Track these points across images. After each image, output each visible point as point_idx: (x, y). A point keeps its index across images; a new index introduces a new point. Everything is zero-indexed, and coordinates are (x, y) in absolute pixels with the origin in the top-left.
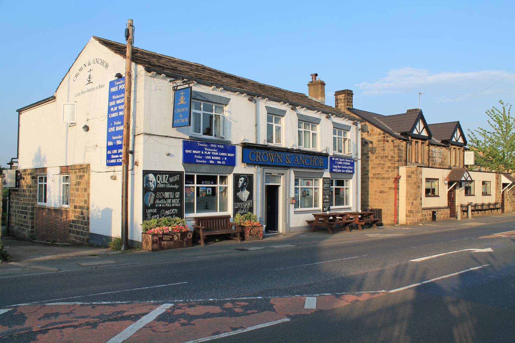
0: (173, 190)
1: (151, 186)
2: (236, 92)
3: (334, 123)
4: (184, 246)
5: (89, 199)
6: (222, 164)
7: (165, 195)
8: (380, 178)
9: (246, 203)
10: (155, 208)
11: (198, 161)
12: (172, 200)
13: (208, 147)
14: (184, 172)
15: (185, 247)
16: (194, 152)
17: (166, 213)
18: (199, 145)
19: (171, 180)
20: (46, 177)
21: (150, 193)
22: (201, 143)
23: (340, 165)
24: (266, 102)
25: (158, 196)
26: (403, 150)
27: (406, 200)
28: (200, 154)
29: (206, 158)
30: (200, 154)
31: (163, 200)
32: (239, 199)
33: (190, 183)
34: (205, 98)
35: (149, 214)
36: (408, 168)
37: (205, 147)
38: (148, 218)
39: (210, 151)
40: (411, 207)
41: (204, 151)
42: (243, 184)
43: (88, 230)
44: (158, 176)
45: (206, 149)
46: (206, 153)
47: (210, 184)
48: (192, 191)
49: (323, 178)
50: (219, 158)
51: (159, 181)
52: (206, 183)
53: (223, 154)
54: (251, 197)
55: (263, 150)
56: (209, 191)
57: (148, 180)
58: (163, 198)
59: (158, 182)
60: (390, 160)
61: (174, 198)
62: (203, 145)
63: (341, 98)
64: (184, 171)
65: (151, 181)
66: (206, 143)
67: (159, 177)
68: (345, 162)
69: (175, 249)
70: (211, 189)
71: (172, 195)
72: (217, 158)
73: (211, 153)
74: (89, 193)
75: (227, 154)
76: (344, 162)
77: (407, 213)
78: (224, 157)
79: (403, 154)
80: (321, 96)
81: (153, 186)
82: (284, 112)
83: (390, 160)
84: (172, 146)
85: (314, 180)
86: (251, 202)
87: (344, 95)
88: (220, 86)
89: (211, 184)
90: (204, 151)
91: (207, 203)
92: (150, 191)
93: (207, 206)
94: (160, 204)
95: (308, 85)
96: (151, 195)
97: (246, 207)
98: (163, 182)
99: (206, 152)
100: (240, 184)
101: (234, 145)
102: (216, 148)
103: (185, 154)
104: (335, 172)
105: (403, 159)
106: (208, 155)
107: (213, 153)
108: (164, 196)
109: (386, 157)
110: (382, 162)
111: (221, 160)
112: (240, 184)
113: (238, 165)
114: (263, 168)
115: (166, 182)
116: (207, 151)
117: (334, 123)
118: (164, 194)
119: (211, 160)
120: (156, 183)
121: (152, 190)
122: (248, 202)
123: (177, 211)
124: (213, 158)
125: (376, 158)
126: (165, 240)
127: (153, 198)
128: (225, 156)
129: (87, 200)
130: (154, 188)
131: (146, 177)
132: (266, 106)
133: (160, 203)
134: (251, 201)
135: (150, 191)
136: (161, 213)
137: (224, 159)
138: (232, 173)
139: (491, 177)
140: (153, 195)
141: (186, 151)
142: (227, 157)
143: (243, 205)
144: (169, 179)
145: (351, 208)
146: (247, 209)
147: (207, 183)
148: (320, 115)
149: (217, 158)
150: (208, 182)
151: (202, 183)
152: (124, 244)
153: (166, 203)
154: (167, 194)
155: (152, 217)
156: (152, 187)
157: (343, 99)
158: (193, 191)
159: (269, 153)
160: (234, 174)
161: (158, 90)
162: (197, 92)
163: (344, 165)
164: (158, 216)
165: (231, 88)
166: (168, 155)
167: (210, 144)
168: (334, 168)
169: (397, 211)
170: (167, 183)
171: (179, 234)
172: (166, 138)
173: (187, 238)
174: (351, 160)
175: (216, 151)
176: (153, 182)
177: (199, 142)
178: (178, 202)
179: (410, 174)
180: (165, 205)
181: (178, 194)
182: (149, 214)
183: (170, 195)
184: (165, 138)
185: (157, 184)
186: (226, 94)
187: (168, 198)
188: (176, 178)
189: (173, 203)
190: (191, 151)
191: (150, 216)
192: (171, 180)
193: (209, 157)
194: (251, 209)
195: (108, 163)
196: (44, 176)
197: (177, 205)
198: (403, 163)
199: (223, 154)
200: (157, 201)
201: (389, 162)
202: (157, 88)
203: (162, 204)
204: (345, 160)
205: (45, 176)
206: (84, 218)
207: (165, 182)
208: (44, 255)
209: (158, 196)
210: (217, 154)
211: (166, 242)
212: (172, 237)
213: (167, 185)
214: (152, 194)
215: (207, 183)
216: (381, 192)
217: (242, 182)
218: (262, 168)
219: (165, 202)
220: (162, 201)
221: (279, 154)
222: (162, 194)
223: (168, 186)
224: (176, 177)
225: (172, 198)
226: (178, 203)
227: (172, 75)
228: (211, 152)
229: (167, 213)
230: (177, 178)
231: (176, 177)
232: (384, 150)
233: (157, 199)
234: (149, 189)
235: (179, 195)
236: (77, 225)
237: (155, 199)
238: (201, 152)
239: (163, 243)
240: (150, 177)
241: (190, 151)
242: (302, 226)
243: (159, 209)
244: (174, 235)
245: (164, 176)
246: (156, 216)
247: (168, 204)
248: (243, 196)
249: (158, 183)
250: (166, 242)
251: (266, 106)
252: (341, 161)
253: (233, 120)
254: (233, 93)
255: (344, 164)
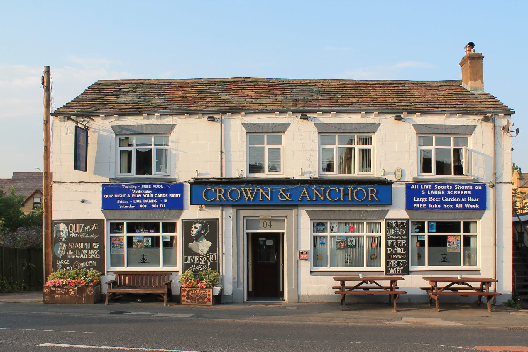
0: (91, 241)
1: (62, 236)
2: (184, 114)
3: (416, 126)
4: (84, 302)
6: (159, 208)
7: (79, 246)
9: (206, 257)
10: (67, 259)
11: (122, 207)
12: (88, 252)
13: (137, 189)
14: (104, 220)
15: (84, 303)
16: (116, 196)
17: (81, 265)
18: (123, 188)
19: (87, 229)
21: (61, 244)
22: (126, 185)
24: (243, 118)
25: (70, 247)
28: (126, 199)
29: (134, 202)
30: (126, 199)
31: (77, 251)
32: (193, 251)
33: (118, 232)
34: (134, 131)
35: (59, 265)
37: (133, 189)
38: (59, 270)
39: (140, 194)
41: (131, 194)
42: (199, 232)
44: (71, 225)
45: (134, 192)
46: (145, 196)
47: (148, 232)
48: (121, 241)
49: (386, 219)
50: (156, 201)
51: (72, 231)
52: (142, 231)
53: (162, 196)
54: (214, 249)
55: (228, 185)
56: (147, 241)
57: (58, 230)
58: (77, 249)
59: (71, 232)
61: (92, 249)
62: (130, 187)
64: (104, 218)
65: (62, 231)
66: (134, 185)
67: (71, 227)
70: (150, 239)
71: (89, 246)
72: (151, 201)
73: (142, 196)
75: (168, 195)
78: (163, 199)
80: (470, 80)
81: (65, 236)
82: (286, 126)
84: (88, 192)
85: (365, 223)
86: (214, 256)
88: (154, 112)
89: (151, 233)
90: (131, 194)
91: (144, 255)
92: (61, 241)
93: (144, 259)
94: (74, 255)
96: (62, 246)
97: (206, 261)
98: (77, 232)
99: (133, 196)
100: (193, 232)
101: (182, 182)
102: (149, 189)
103: (103, 199)
104: (416, 209)
106: (138, 199)
107: (144, 196)
108: (78, 246)
111: (158, 204)
112: (193, 232)
113: (189, 208)
114: (237, 210)
115: (81, 232)
116: (136, 194)
117: (416, 126)
118: (78, 245)
119: (143, 203)
120: (68, 233)
121: (63, 240)
122: (209, 255)
123: (95, 263)
124: (145, 201)
126: (58, 294)
127: (64, 248)
128: (165, 198)
130: (65, 238)
131: (56, 227)
132: (243, 124)
133: (72, 254)
134: (215, 255)
135: (61, 241)
136: (74, 265)
137: (163, 201)
138: (179, 218)
140: (65, 245)
141: (106, 196)
142: (168, 198)
143: (199, 259)
144: (84, 228)
145: (481, 271)
146: (207, 265)
147: (144, 232)
148: (375, 118)
149: (151, 201)
150: (145, 230)
151: (136, 231)
153: (81, 255)
154: (82, 245)
155: (63, 269)
156: (64, 237)
158: (459, 240)
159: (243, 189)
160: (182, 219)
161: (69, 133)
162: (122, 126)
164: (71, 268)
165: (172, 112)
166: (83, 202)
167: (140, 185)
170: (82, 233)
171: (76, 288)
172: (80, 183)
173: (87, 294)
174: (446, 185)
175: (149, 192)
176: (64, 232)
177: (123, 185)
178: (96, 253)
180: (80, 256)
181: (96, 245)
182: (59, 265)
183: (85, 246)
184: (79, 184)
185: (70, 233)
186: (167, 121)
187: (83, 249)
188: (94, 227)
189: (89, 255)
190: (112, 195)
191: (61, 268)
192: (87, 229)
193: (140, 201)
194: (215, 266)
195: (477, 206)
197: (94, 257)
199: (162, 196)
200: (70, 252)
202: (69, 132)
203: (75, 255)
207: (79, 232)
208: (253, 307)
209: (70, 247)
210: (152, 196)
211: (59, 295)
212: (67, 291)
213: (82, 235)
214: (63, 245)
215: (144, 231)
217: (198, 229)
218: (235, 210)
219: (79, 253)
220: (76, 252)
221: (262, 188)
222: (75, 244)
223: (84, 236)
224: (94, 226)
225: (88, 250)
226: (97, 255)
227: (82, 114)
228: (142, 194)
229: (82, 265)
230: (94, 227)
231: (94, 226)
233: (70, 250)
234: (59, 239)
235: (98, 246)
237: (67, 250)
238: (126, 196)
239: (56, 296)
240: (61, 227)
241: (111, 196)
242: (330, 294)
243: (72, 261)
244: (69, 288)
245: (78, 225)
246: (69, 268)
247: (83, 255)
248: (200, 248)
249: (71, 233)
250: (59, 296)
251: (243, 124)
253: (179, 151)
254: (180, 117)
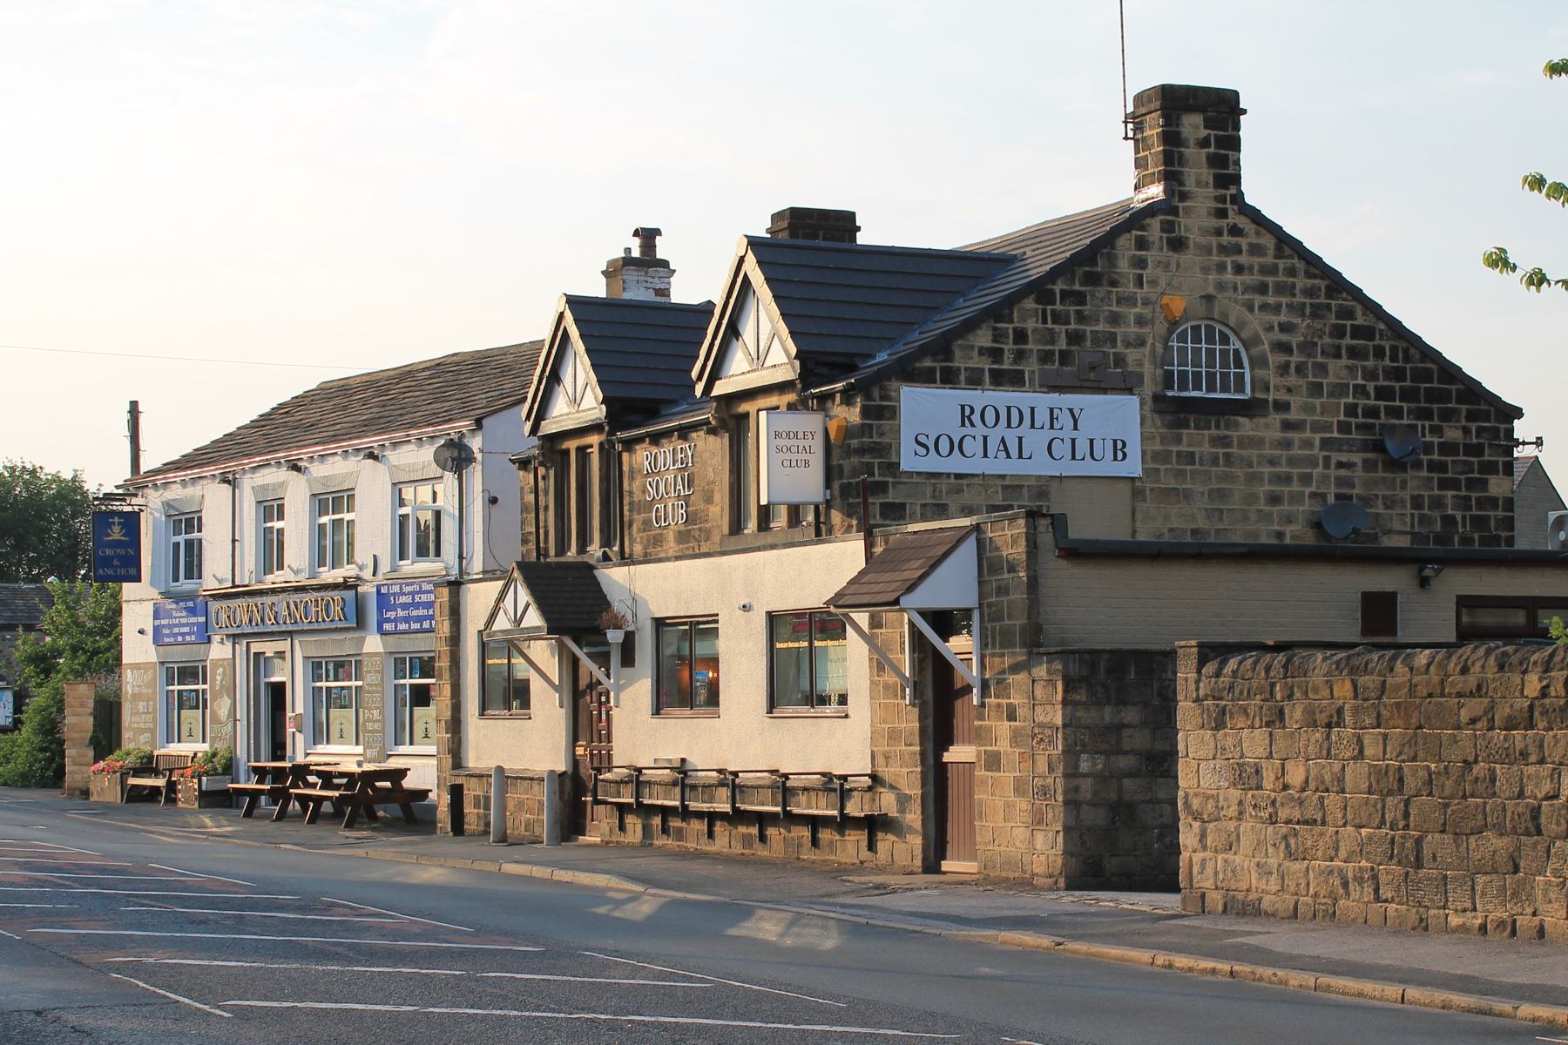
20: (283, 505)
23: (405, 606)
68: (420, 592)
69: (1519, 980)
76: (418, 593)
95: (602, 272)
163: (416, 606)
168: (388, 620)
169: (1171, 695)
196: (275, 504)
204: (421, 587)
205: (280, 502)
252: (409, 593)
255: (417, 600)
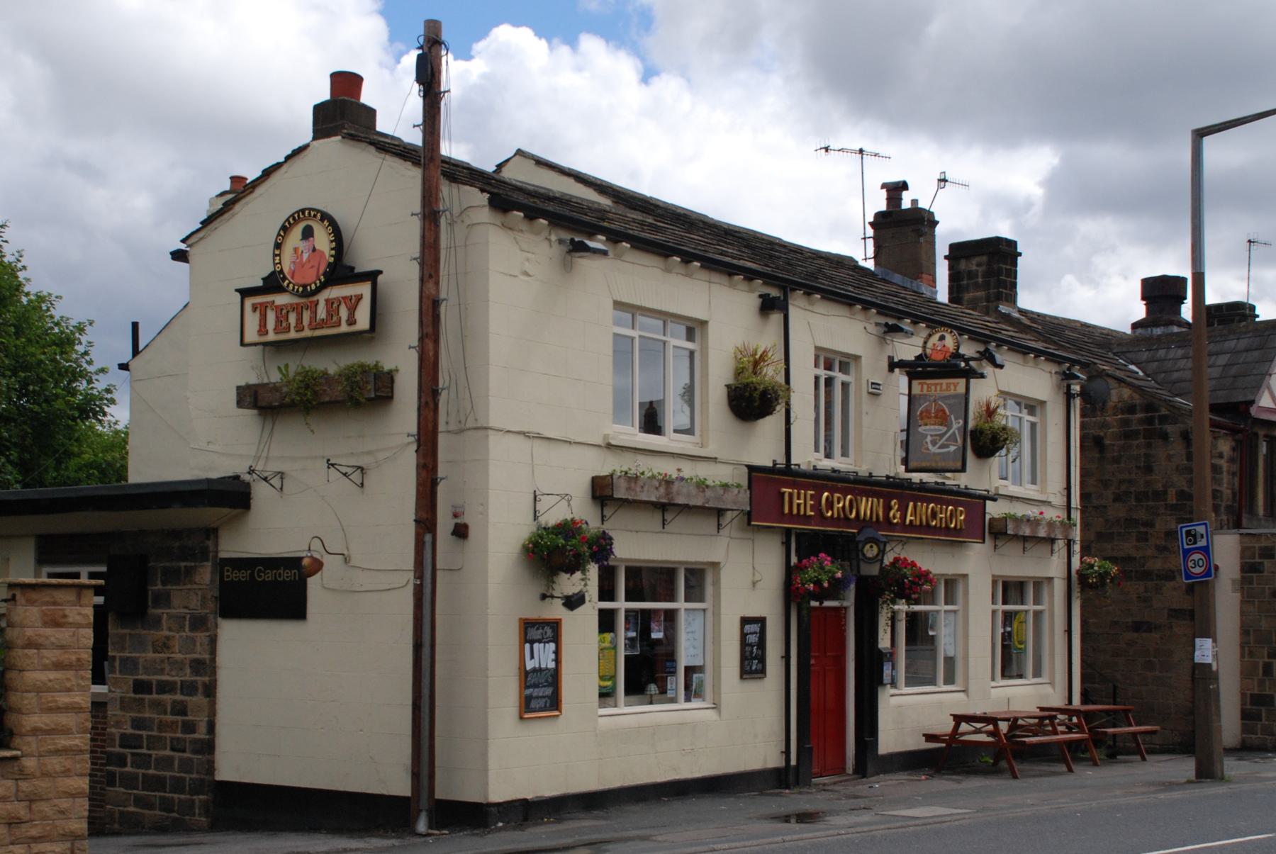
5: (213, 660)
8: (1133, 574)
26: (1225, 469)
27: (1242, 656)
36: (1246, 539)
40: (1261, 683)
43: (210, 768)
60: (1173, 508)
63: (974, 268)
74: (216, 636)
77: (1249, 707)
79: (1225, 485)
83: (1173, 508)
87: (984, 258)
105: (1224, 504)
109: (1160, 495)
110: (1142, 515)
125: (1115, 500)
129: (208, 662)
139: (1171, 502)
152: (427, 811)
157: (980, 274)
179: (1257, 560)
198: (1224, 517)
201: (1171, 515)
206: (190, 727)
216: (1137, 627)
232: (1149, 469)
236: (150, 756)
